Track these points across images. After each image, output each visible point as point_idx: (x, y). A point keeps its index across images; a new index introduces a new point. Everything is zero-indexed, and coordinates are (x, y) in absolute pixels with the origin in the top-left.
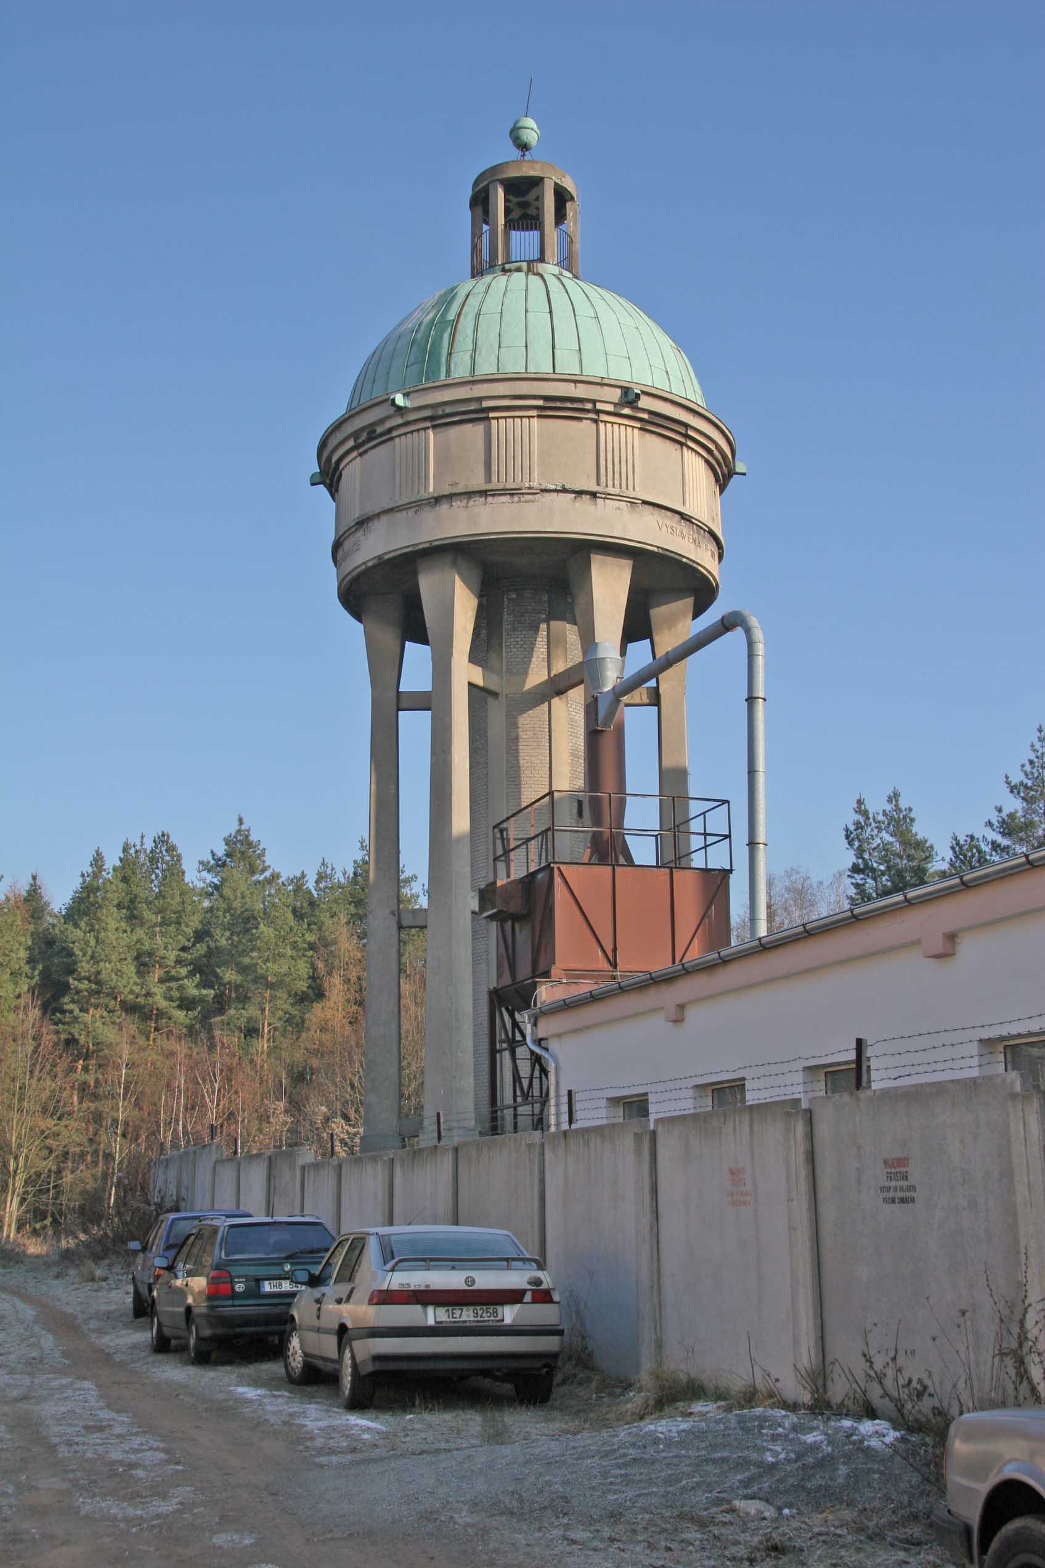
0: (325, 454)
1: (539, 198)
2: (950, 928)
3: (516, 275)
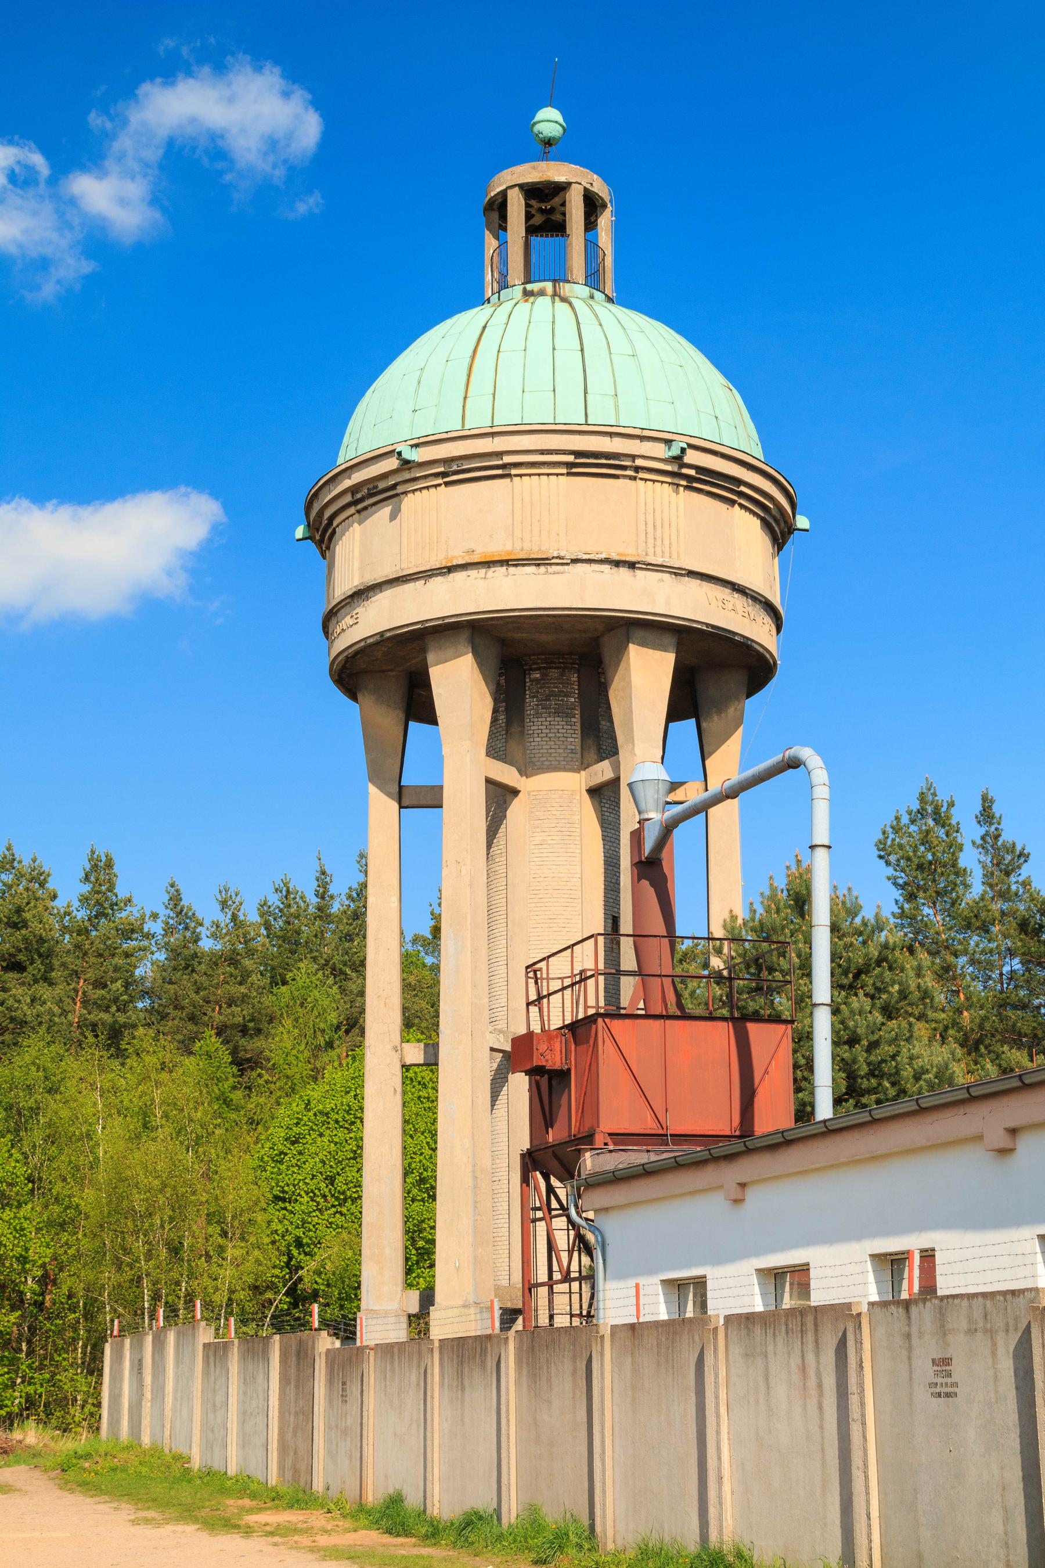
2: (1011, 1124)
3: (540, 299)
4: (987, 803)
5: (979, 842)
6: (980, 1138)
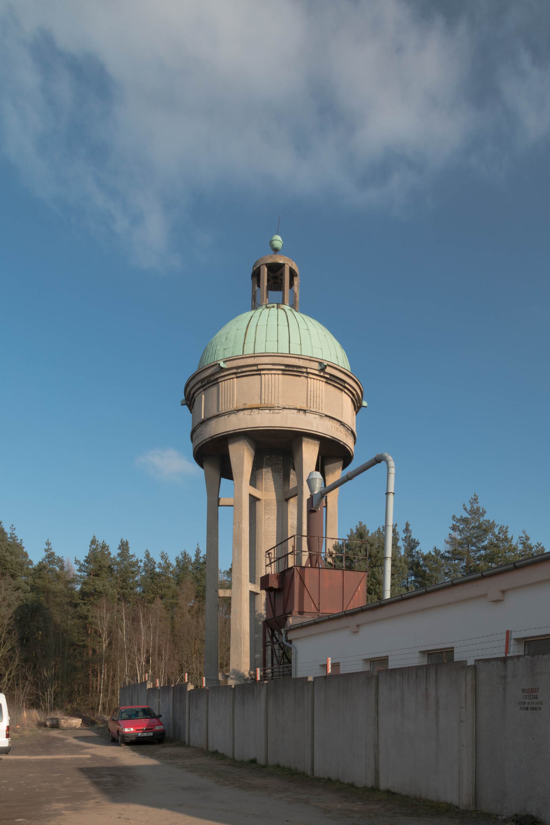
0: (188, 390)
1: (282, 274)
3: (272, 309)
4: (407, 525)
5: (404, 538)
6: (485, 595)
